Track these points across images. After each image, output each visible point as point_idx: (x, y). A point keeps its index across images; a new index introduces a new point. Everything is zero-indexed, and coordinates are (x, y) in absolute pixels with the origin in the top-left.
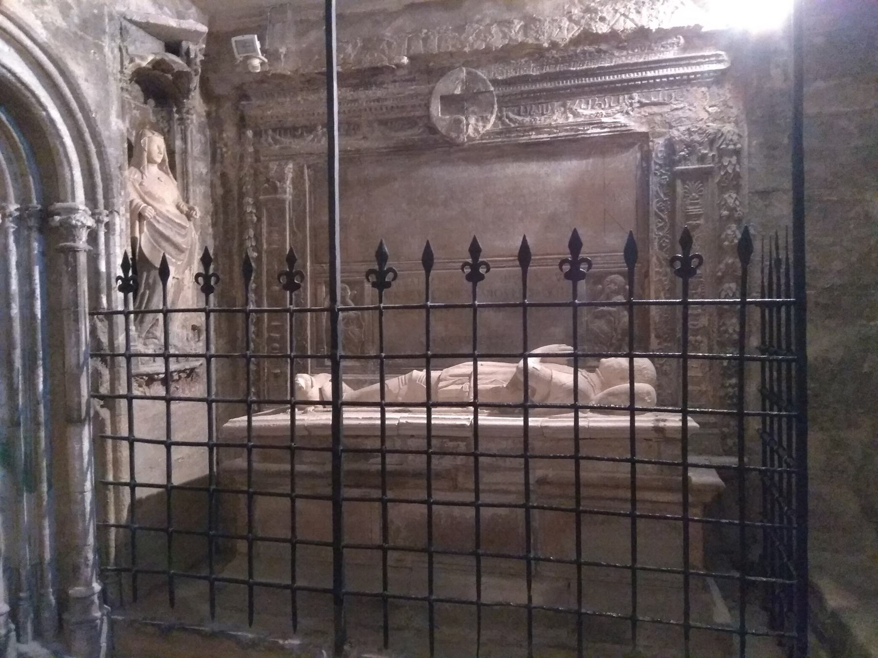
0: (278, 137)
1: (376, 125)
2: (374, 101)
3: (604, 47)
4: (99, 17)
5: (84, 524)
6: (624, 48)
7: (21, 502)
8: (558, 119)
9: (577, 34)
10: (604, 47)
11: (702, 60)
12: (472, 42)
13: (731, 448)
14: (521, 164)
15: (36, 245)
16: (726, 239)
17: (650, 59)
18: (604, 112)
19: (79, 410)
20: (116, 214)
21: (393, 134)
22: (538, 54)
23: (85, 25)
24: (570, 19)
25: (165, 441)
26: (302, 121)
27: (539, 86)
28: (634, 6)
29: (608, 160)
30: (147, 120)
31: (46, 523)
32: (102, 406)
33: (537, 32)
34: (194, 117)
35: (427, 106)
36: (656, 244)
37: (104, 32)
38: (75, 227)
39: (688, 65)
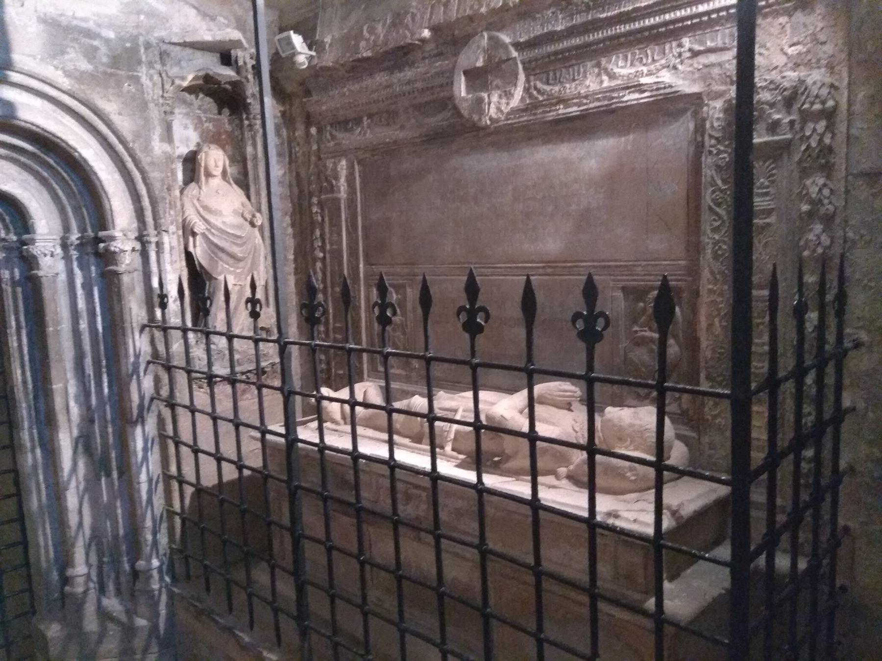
1: (411, 110)
2: (406, 84)
7: (100, 484)
8: (590, 84)
14: (550, 146)
15: (93, 268)
18: (645, 69)
20: (164, 233)
23: (115, 61)
25: (222, 436)
27: (565, 44)
29: (652, 134)
30: (222, 131)
31: (118, 504)
35: (451, 84)
36: (709, 251)
37: (140, 62)
38: (115, 253)
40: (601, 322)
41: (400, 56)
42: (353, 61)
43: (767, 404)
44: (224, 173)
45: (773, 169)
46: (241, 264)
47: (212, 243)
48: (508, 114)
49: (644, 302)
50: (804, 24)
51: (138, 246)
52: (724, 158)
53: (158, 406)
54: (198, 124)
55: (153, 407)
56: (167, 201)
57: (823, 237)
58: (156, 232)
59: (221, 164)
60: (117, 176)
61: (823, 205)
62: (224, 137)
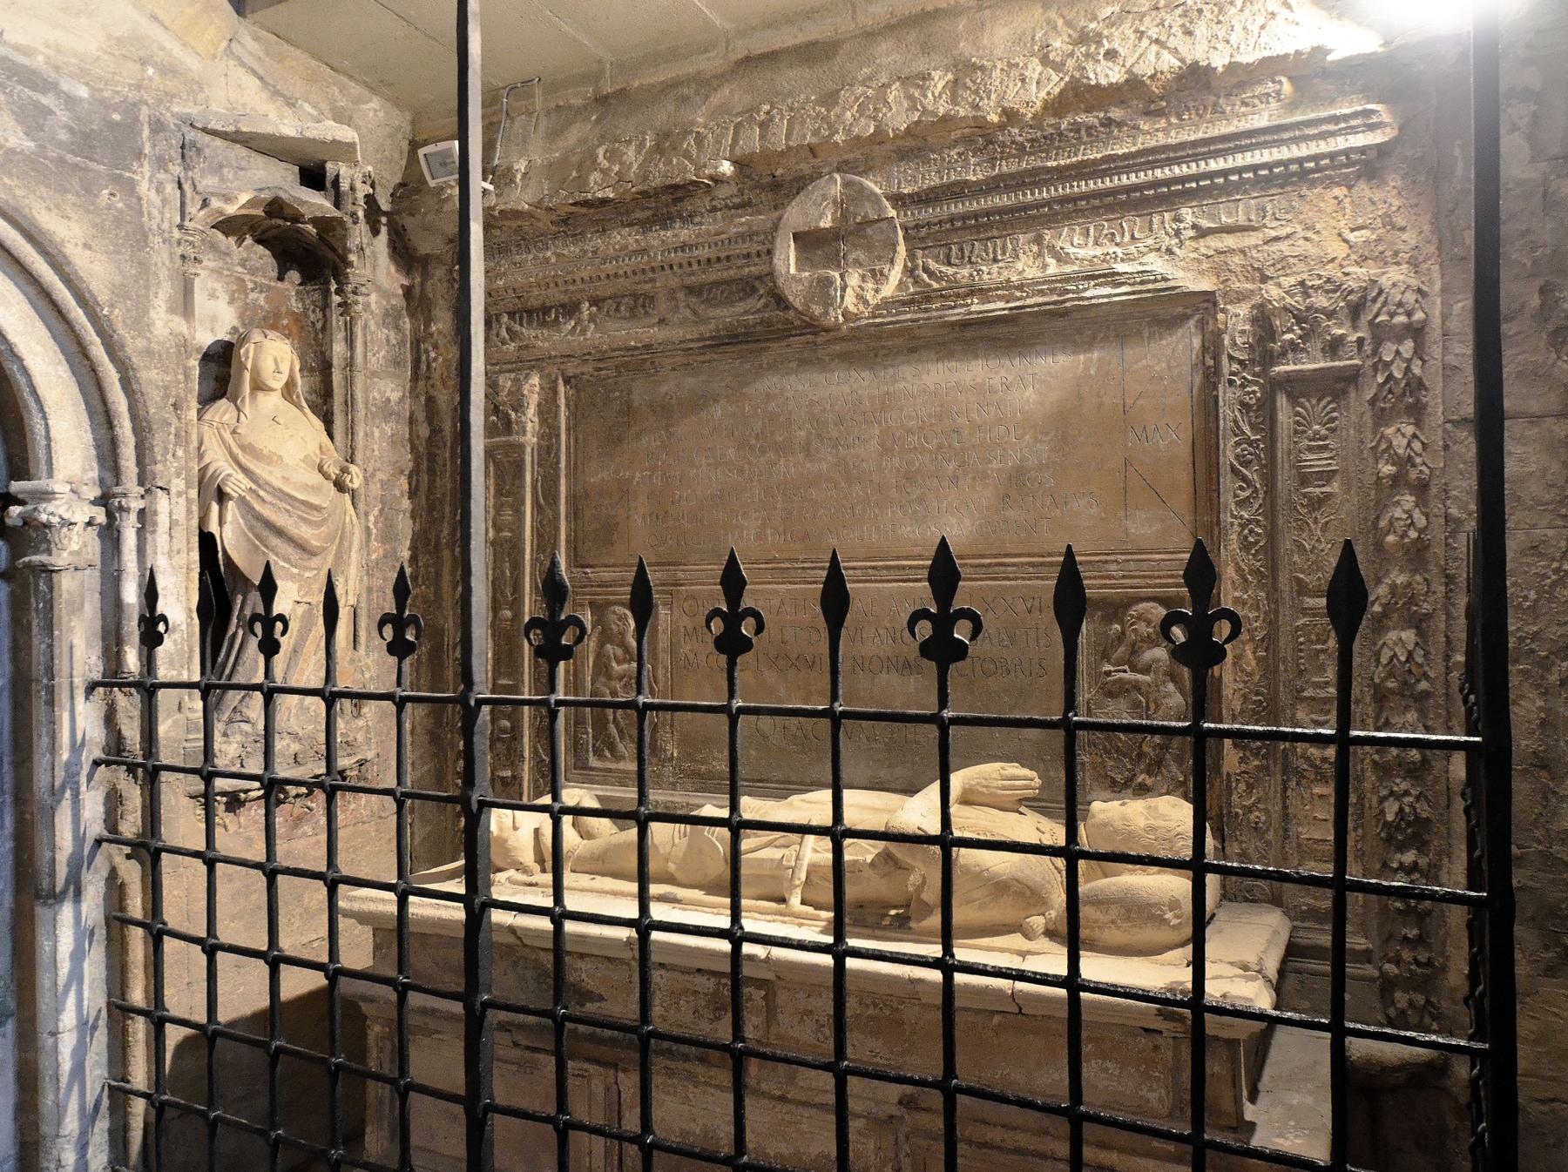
0: (517, 327)
1: (681, 295)
3: (1116, 113)
4: (129, 128)
5: (57, 1096)
6: (1160, 113)
8: (1023, 268)
9: (1057, 90)
10: (1116, 113)
11: (1331, 127)
12: (852, 122)
13: (1403, 1012)
16: (1391, 528)
17: (1216, 133)
18: (1119, 251)
19: (52, 874)
21: (711, 312)
22: (981, 137)
23: (85, 142)
24: (1045, 61)
25: (280, 908)
26: (556, 296)
27: (985, 203)
28: (1180, 21)
29: (1130, 353)
30: (283, 309)
32: (128, 857)
33: (976, 92)
34: (373, 297)
36: (1234, 537)
37: (139, 155)
38: (48, 526)
39: (1296, 140)
40: (1225, 628)
41: (668, 202)
42: (574, 204)
43: (1515, 758)
44: (288, 390)
45: (1334, 410)
46: (315, 562)
47: (259, 518)
48: (877, 307)
49: (1122, 623)
50: (1370, 200)
51: (101, 518)
52: (1254, 392)
53: (110, 858)
54: (238, 291)
55: (100, 859)
56: (173, 430)
57: (1417, 514)
58: (142, 490)
59: (285, 368)
60: (64, 371)
61: (1414, 465)
62: (285, 322)
